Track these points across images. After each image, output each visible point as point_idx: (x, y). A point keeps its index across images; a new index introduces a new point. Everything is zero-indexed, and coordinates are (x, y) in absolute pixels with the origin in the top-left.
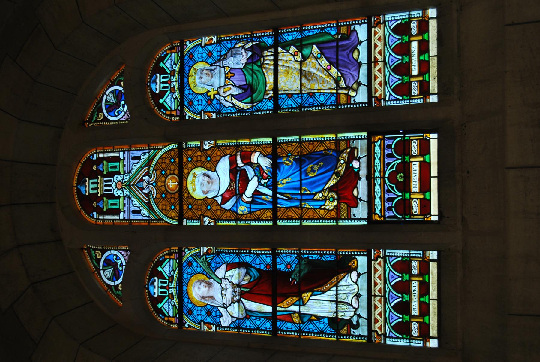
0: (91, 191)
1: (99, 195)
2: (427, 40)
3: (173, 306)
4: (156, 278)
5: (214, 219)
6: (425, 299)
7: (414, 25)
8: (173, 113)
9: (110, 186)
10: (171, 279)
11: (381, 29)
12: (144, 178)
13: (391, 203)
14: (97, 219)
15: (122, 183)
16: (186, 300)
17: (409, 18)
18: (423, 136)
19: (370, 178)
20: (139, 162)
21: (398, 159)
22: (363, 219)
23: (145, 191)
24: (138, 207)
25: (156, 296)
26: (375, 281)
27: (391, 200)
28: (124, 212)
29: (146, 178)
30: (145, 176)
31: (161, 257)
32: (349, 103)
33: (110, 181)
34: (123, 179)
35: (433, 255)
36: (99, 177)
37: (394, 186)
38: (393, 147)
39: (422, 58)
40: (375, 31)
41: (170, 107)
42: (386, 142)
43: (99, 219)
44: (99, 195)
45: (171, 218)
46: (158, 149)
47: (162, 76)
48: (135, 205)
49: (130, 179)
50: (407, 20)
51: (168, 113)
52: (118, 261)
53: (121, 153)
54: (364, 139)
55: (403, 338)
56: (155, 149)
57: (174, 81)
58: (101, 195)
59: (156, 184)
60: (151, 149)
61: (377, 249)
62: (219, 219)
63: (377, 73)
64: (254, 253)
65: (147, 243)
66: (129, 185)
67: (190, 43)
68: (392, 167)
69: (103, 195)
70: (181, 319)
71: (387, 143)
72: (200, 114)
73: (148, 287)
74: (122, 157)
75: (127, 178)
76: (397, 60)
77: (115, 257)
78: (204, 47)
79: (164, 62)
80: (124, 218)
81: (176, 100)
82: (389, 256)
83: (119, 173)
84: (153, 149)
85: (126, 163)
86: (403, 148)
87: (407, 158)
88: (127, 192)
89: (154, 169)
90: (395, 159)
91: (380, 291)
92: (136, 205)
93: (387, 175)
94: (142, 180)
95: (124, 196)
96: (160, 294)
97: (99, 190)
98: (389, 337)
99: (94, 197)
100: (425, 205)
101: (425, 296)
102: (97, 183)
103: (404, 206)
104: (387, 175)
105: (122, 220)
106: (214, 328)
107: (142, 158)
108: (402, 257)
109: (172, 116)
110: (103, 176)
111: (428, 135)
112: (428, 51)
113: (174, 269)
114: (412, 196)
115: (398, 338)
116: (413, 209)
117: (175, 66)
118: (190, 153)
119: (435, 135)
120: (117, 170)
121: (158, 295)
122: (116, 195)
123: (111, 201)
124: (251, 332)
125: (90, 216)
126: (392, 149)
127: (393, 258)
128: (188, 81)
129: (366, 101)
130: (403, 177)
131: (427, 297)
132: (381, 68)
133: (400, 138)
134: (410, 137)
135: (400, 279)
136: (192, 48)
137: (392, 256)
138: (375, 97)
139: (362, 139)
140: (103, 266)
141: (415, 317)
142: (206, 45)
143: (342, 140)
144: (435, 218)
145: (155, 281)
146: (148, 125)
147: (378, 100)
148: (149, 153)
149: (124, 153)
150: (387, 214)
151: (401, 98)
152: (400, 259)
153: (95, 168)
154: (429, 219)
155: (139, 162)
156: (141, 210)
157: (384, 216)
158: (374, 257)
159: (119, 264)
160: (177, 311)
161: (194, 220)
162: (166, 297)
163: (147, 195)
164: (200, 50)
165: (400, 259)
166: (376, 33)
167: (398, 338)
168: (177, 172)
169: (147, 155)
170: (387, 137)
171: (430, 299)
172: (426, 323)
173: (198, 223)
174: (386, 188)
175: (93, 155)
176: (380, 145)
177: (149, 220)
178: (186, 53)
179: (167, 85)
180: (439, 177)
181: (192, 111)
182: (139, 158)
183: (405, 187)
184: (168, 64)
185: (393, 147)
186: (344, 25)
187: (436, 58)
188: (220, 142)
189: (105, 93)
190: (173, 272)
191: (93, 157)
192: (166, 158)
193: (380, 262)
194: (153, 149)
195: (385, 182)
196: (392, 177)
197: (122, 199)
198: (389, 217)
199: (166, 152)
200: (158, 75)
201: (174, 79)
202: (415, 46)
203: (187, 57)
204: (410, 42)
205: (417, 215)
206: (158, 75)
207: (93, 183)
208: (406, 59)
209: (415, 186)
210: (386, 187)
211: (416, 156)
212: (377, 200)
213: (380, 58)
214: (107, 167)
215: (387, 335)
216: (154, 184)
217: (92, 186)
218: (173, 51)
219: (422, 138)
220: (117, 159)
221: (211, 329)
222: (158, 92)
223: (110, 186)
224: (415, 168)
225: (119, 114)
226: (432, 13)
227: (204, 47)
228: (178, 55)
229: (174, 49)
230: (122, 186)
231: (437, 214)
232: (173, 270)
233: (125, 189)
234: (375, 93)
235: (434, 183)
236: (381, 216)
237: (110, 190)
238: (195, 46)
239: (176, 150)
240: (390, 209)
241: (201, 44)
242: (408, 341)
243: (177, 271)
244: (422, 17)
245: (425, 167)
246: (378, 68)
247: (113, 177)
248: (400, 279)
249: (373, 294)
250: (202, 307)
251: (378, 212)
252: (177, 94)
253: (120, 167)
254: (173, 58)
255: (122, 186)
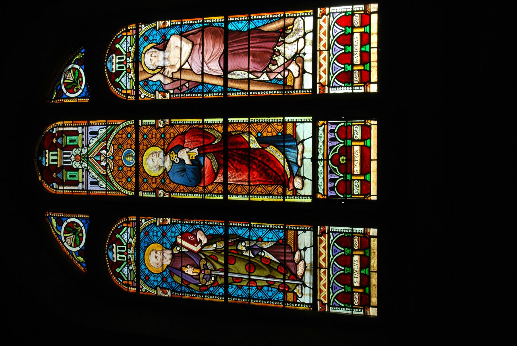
0: (51, 163)
1: (59, 167)
2: (369, 180)
3: (130, 79)
4: (114, 245)
5: (169, 192)
6: (366, 48)
7: (357, 19)
8: (128, 92)
9: (69, 158)
10: (128, 53)
11: (325, 238)
12: (101, 152)
13: (333, 183)
14: (56, 189)
15: (80, 156)
16: (143, 267)
17: (353, 11)
18: (365, 122)
19: (315, 160)
20: (97, 137)
21: (341, 143)
22: (308, 196)
23: (104, 164)
24: (95, 178)
25: (115, 261)
26: (320, 288)
27: (333, 180)
28: (82, 183)
29: (104, 152)
30: (102, 149)
31: (119, 225)
32: (295, 302)
33: (69, 154)
34: (81, 152)
35: (373, 232)
36: (59, 149)
37: (337, 168)
38: (336, 131)
39: (363, 49)
40: (320, 239)
41: (126, 87)
42: (329, 127)
43: (58, 189)
44: (59, 167)
45: (127, 189)
46: (115, 125)
47: (117, 57)
48: (93, 177)
49: (88, 152)
50: (351, 13)
51: (124, 92)
52: (79, 85)
53: (80, 128)
54: (310, 122)
55: (345, 307)
56: (112, 125)
57: (129, 63)
58: (60, 166)
59: (114, 158)
60: (109, 125)
61: (323, 225)
62: (173, 192)
63: (323, 24)
64: (207, 224)
65: (103, 213)
66: (87, 158)
67: (146, 221)
68: (335, 150)
69: (62, 167)
70: (137, 90)
71: (330, 128)
72: (156, 289)
73: (107, 252)
74: (80, 132)
75: (85, 151)
76: (340, 251)
77: (75, 225)
78: (158, 30)
79: (120, 43)
80: (83, 188)
81: (132, 80)
82: (333, 232)
83: (77, 147)
84: (110, 125)
85: (84, 136)
86: (346, 133)
87: (349, 177)
88: (85, 165)
89: (111, 143)
90: (338, 143)
91: (324, 46)
92: (93, 176)
93: (330, 158)
94: (99, 154)
95: (82, 168)
96: (118, 259)
97: (58, 162)
98: (333, 306)
99: (54, 169)
100: (366, 185)
101: (366, 45)
102: (57, 155)
103: (346, 186)
104: (330, 158)
105: (80, 190)
106: (169, 294)
107: (99, 133)
108: (346, 233)
109: (127, 95)
110: (63, 149)
111: (369, 121)
112: (369, 43)
113: (131, 45)
114: (353, 178)
115: (341, 307)
116: (354, 134)
117: (130, 48)
118: (145, 130)
119: (375, 122)
120: (76, 143)
121: (116, 71)
122: (74, 167)
123: (69, 173)
124: (203, 96)
125: (49, 186)
126: (335, 133)
127: (337, 14)
128: (144, 257)
129: (311, 87)
130: (345, 160)
131: (367, 266)
132: (325, 56)
133: (343, 124)
134: (352, 123)
135: (343, 290)
136: (147, 31)
137: (336, 232)
138: (320, 83)
139: (307, 122)
140: (64, 233)
141: (356, 287)
142: (160, 28)
143: (289, 122)
144: (374, 198)
145: (113, 247)
146: (105, 103)
147: (323, 86)
148: (106, 128)
149: (83, 128)
150: (330, 194)
151: (343, 85)
152: (343, 234)
153: (54, 141)
154: (369, 199)
155: (97, 137)
156: (98, 182)
157: (327, 195)
158: (320, 233)
159: (79, 230)
160: (134, 84)
161: (149, 192)
162: (124, 262)
163: (105, 167)
164: (155, 32)
165: (343, 234)
166: (321, 241)
167: (341, 307)
168: (133, 147)
169: (105, 130)
170: (330, 123)
171: (370, 48)
172: (367, 32)
173: (153, 195)
174: (329, 169)
175: (53, 129)
176: (324, 130)
177: (106, 191)
178: (141, 34)
179: (124, 256)
180: (379, 160)
181: (147, 91)
182: (96, 133)
183: (347, 168)
184: (124, 46)
185: (336, 131)
186: (291, 229)
187: (376, 49)
188: (173, 121)
189: (63, 71)
190: (131, 239)
191: (53, 130)
192: (122, 134)
193: (325, 19)
194: (110, 125)
195: (328, 163)
196: (335, 160)
197: (80, 170)
198: (331, 196)
199: (123, 128)
200: (114, 55)
201: (130, 60)
202: (357, 37)
203: (142, 38)
204: (352, 256)
205: (358, 195)
206: (114, 55)
207: (52, 155)
208: (349, 49)
209: (357, 169)
210: (329, 168)
211: (358, 141)
212: (321, 181)
213: (325, 265)
214: (67, 140)
215: (331, 304)
216: (112, 158)
217: (52, 158)
218: (129, 34)
219: (363, 124)
220: (76, 133)
221: (167, 293)
222: (114, 71)
223: (69, 158)
224: (356, 150)
225: (77, 92)
226: (374, 7)
227: (158, 30)
228: (134, 230)
229: (129, 31)
230: (79, 158)
231: (376, 159)
232: (131, 237)
233: (83, 161)
234: (320, 79)
235: (374, 165)
236: (324, 195)
237: (69, 163)
238: (150, 225)
239: (133, 126)
240: (332, 189)
241: (155, 27)
242: (351, 88)
243: (135, 237)
244: (364, 11)
245: (365, 151)
246: (323, 56)
247: (72, 151)
248: (343, 290)
249: (318, 49)
250: (158, 274)
251: (321, 191)
252: (132, 75)
253: (79, 140)
254: (129, 40)
255: (79, 158)
